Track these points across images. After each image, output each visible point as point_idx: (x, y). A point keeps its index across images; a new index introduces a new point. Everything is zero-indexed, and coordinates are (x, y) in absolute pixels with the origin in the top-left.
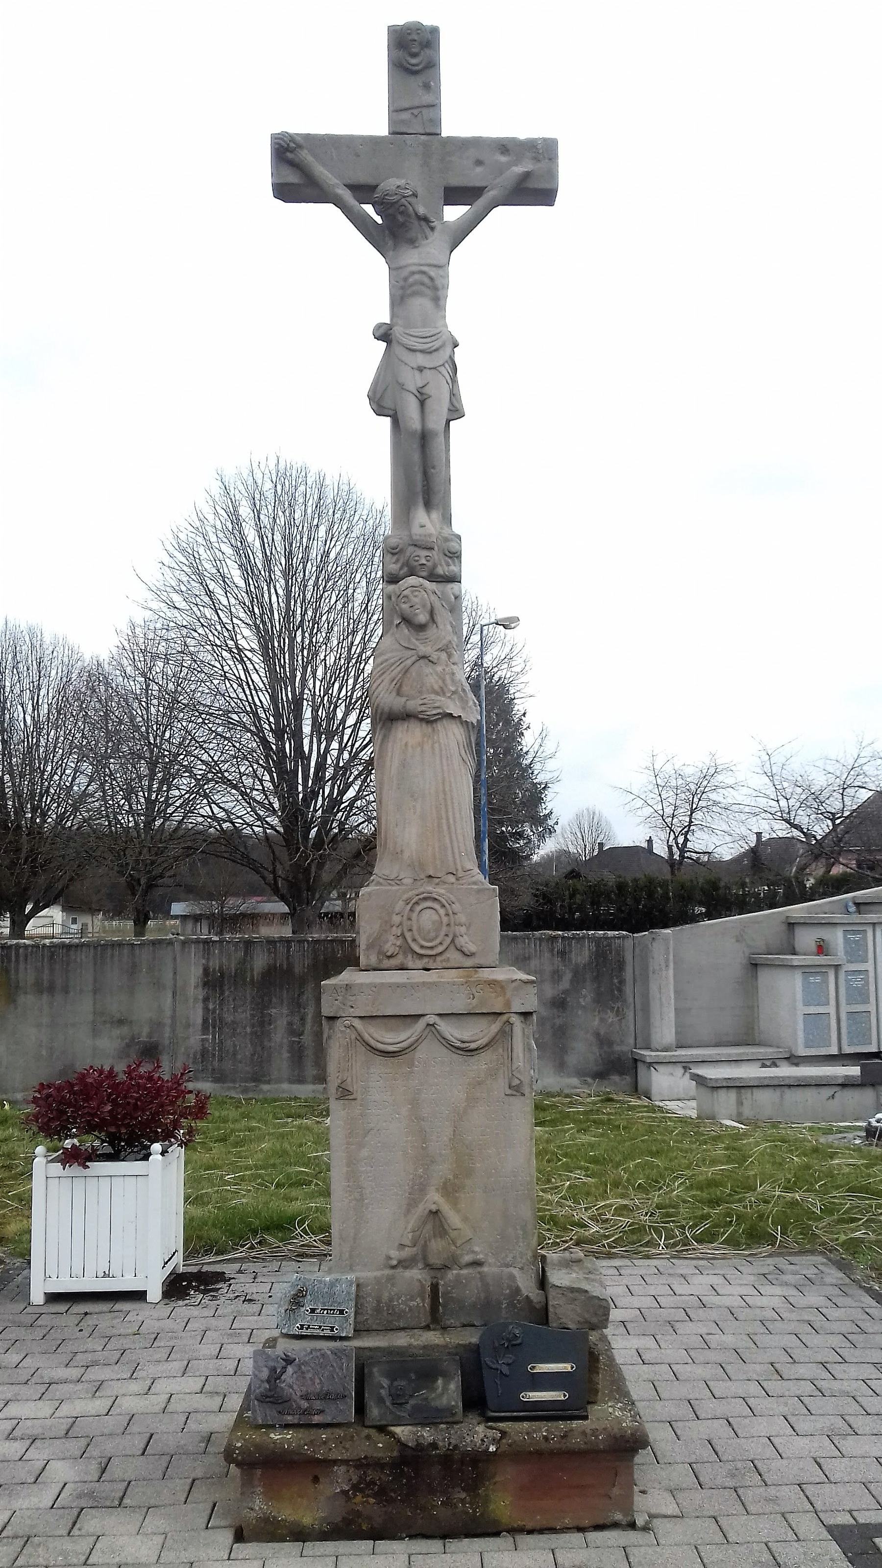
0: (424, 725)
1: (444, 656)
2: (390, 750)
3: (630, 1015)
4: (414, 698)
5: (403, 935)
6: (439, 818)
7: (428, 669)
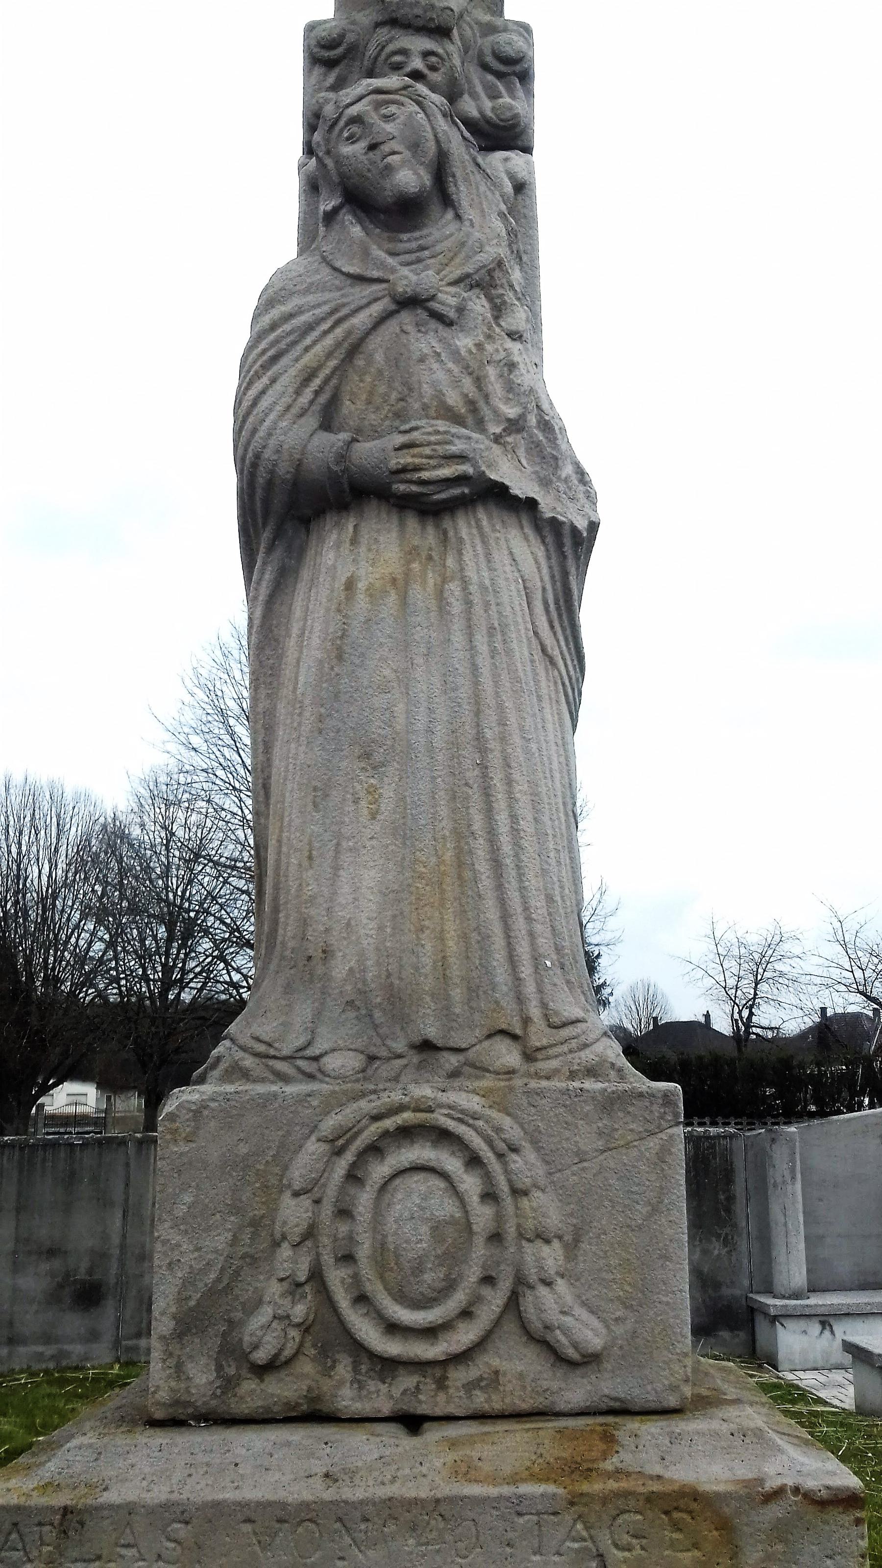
0: (412, 523)
1: (479, 305)
2: (298, 612)
3: (743, 1245)
4: (376, 433)
5: (317, 1275)
6: (461, 834)
7: (425, 342)
